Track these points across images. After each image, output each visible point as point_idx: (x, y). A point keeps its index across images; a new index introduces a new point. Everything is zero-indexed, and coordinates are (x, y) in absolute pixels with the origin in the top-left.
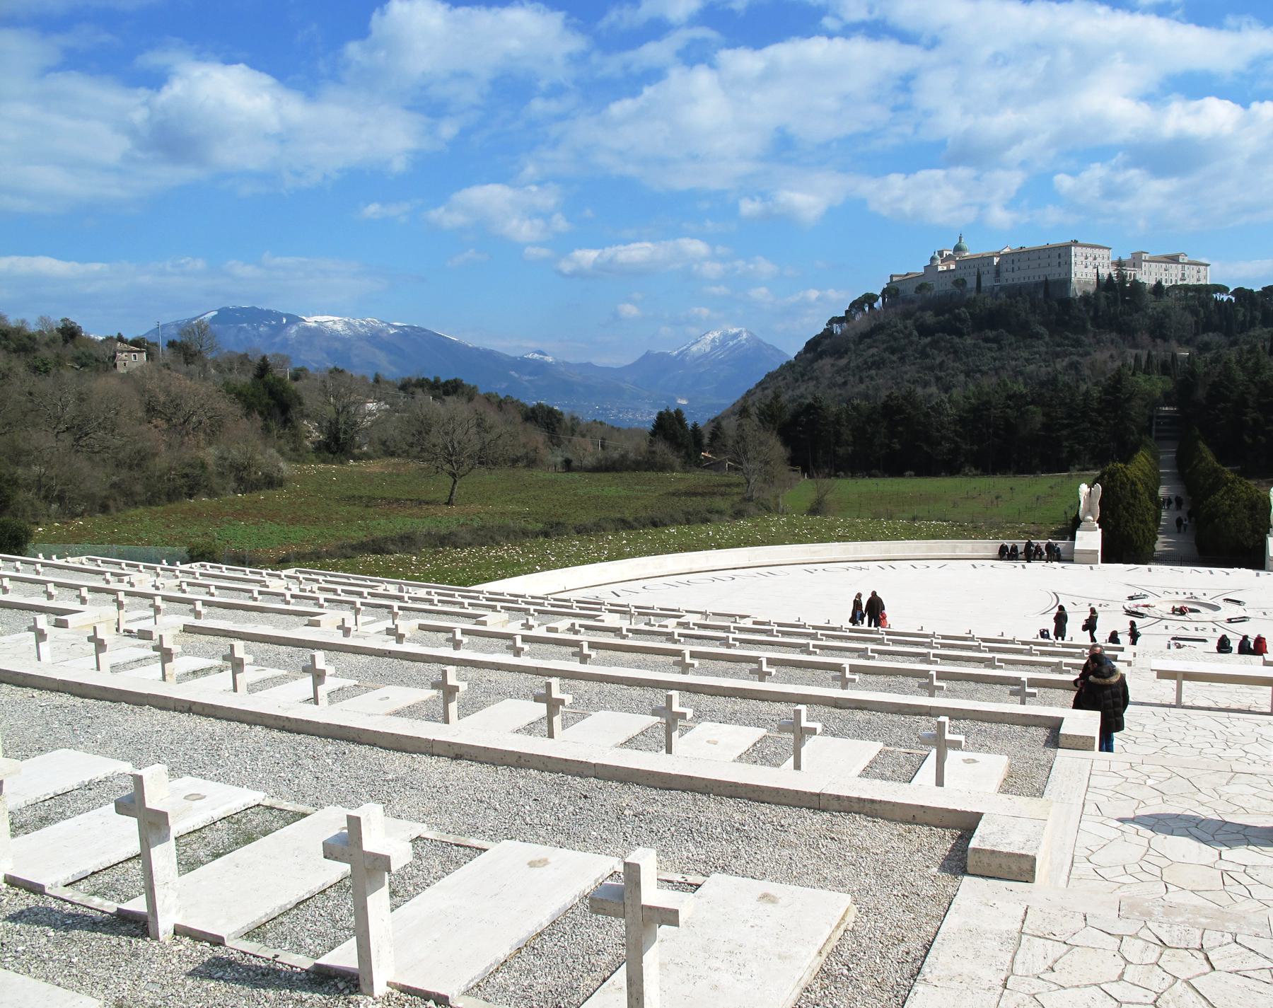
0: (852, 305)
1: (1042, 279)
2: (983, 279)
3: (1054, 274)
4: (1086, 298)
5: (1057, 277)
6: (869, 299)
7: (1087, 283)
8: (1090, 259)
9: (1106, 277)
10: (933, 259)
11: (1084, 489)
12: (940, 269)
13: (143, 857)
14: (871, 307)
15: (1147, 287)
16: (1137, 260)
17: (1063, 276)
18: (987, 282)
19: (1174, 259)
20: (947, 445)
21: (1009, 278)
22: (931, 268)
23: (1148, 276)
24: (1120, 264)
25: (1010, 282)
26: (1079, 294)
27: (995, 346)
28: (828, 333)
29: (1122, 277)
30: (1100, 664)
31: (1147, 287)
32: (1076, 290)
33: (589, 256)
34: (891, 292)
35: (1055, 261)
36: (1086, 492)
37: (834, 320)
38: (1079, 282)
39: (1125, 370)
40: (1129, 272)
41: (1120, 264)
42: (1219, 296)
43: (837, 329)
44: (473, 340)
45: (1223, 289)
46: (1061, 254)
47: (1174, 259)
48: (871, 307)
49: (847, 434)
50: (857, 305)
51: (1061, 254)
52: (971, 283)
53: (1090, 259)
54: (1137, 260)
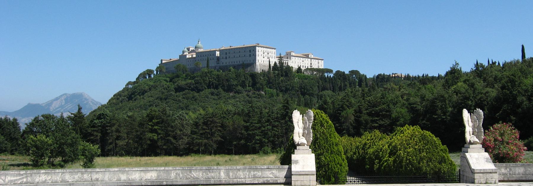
0: (141, 75)
1: (241, 63)
2: (210, 61)
4: (263, 73)
6: (149, 72)
7: (264, 66)
8: (266, 54)
10: (183, 52)
12: (188, 57)
14: (150, 76)
15: (294, 70)
16: (289, 56)
17: (252, 62)
19: (307, 56)
20: (186, 140)
22: (183, 57)
25: (224, 64)
27: (216, 97)
29: (281, 63)
34: (159, 69)
37: (129, 83)
40: (285, 61)
41: (280, 58)
45: (330, 71)
46: (251, 51)
48: (150, 76)
49: (124, 130)
53: (266, 54)
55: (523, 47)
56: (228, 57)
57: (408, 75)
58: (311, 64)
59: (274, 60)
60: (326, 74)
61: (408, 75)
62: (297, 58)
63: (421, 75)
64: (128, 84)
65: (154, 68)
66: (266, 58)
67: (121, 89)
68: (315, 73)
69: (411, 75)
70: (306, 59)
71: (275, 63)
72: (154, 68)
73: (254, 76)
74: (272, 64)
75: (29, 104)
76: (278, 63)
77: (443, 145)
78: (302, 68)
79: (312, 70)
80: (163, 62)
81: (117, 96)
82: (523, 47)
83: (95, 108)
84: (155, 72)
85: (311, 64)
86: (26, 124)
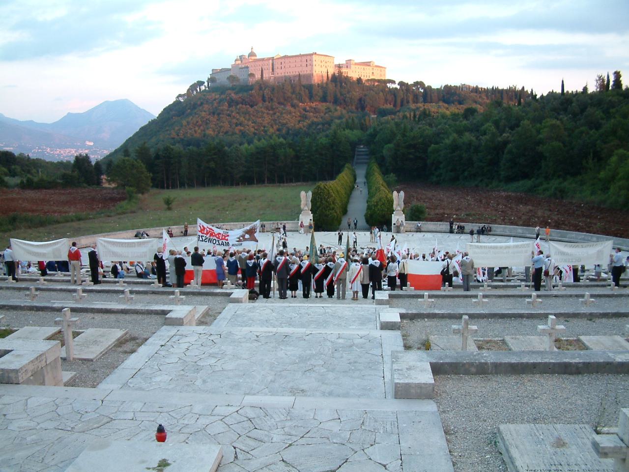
1: (297, 73)
2: (264, 71)
3: (305, 71)
6: (201, 83)
8: (323, 63)
11: (303, 193)
13: (553, 276)
23: (353, 74)
24: (339, 66)
25: (280, 75)
29: (340, 73)
30: (465, 265)
32: (316, 80)
33: (417, 119)
35: (304, 64)
36: (305, 197)
37: (180, 96)
39: (400, 132)
40: (344, 70)
42: (389, 85)
44: (8, 117)
45: (393, 82)
47: (367, 64)
51: (308, 58)
54: (349, 63)
55: (563, 82)
56: (283, 67)
57: (477, 86)
58: (373, 73)
59: (331, 71)
60: (389, 85)
61: (477, 86)
63: (449, 85)
64: (178, 97)
65: (205, 79)
67: (171, 102)
68: (376, 84)
69: (480, 86)
72: (205, 79)
73: (310, 88)
74: (330, 75)
75: (31, 121)
77: (532, 282)
78: (362, 78)
79: (374, 80)
80: (214, 72)
81: (167, 110)
82: (563, 82)
83: (145, 123)
84: (206, 84)
85: (373, 73)
86: (523, 88)
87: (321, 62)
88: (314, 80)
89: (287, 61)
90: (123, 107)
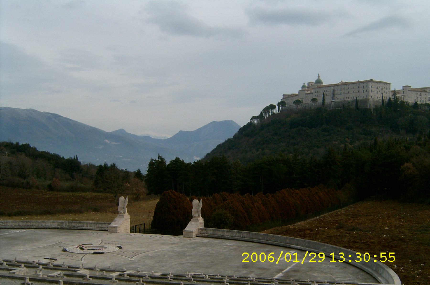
0: (264, 110)
5: (362, 98)
6: (272, 107)
8: (380, 89)
9: (388, 98)
17: (365, 98)
18: (328, 100)
21: (341, 98)
26: (372, 107)
28: (250, 125)
29: (396, 98)
31: (410, 105)
34: (282, 104)
37: (254, 118)
38: (373, 100)
43: (255, 121)
50: (266, 110)
52: (320, 101)
53: (380, 89)
62: (413, 93)
66: (380, 93)
70: (424, 93)
71: (390, 98)
76: (392, 98)
87: (377, 88)
88: (370, 105)
89: (346, 87)
90: (215, 126)
